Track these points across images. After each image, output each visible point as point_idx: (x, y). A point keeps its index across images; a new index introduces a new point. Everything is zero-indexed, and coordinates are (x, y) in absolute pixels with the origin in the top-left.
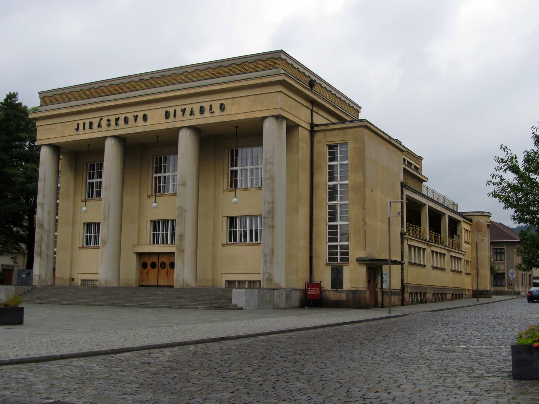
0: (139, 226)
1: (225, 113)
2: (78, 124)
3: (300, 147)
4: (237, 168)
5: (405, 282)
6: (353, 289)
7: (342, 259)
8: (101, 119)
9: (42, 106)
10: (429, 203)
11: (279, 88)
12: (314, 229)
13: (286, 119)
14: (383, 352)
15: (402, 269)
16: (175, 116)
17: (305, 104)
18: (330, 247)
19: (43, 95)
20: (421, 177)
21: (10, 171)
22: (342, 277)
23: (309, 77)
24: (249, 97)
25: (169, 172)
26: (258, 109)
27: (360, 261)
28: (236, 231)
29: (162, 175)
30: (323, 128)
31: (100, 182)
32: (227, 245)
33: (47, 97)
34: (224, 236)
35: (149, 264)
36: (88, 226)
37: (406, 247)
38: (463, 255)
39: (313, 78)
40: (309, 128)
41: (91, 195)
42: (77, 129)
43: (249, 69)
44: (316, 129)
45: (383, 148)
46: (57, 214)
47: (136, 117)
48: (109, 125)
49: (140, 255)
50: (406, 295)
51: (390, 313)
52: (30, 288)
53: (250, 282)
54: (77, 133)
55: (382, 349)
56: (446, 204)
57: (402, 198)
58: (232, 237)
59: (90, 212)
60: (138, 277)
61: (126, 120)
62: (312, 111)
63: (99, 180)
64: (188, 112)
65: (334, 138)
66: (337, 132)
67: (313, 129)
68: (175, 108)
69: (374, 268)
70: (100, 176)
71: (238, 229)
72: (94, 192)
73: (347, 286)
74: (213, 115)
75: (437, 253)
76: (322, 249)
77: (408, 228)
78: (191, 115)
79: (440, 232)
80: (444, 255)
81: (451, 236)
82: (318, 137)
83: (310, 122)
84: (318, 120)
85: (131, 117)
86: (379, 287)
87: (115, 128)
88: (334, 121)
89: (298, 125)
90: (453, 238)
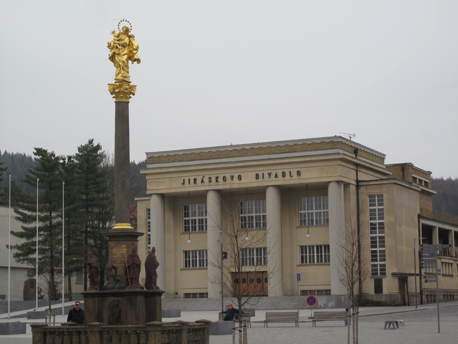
1: (301, 177)
2: (184, 180)
3: (351, 199)
7: (381, 274)
8: (203, 177)
11: (339, 162)
13: (342, 182)
16: (263, 178)
19: (150, 156)
22: (382, 286)
27: (394, 274)
30: (366, 183)
32: (300, 265)
35: (241, 280)
39: (356, 146)
40: (356, 184)
42: (184, 183)
44: (360, 184)
47: (232, 177)
48: (210, 181)
50: (424, 297)
51: (416, 308)
53: (318, 291)
54: (183, 186)
61: (224, 179)
62: (357, 171)
64: (273, 175)
65: (375, 191)
66: (375, 186)
67: (358, 184)
68: (262, 172)
69: (403, 279)
73: (385, 291)
75: (446, 263)
76: (368, 266)
78: (275, 177)
80: (452, 264)
82: (362, 190)
85: (228, 177)
86: (406, 292)
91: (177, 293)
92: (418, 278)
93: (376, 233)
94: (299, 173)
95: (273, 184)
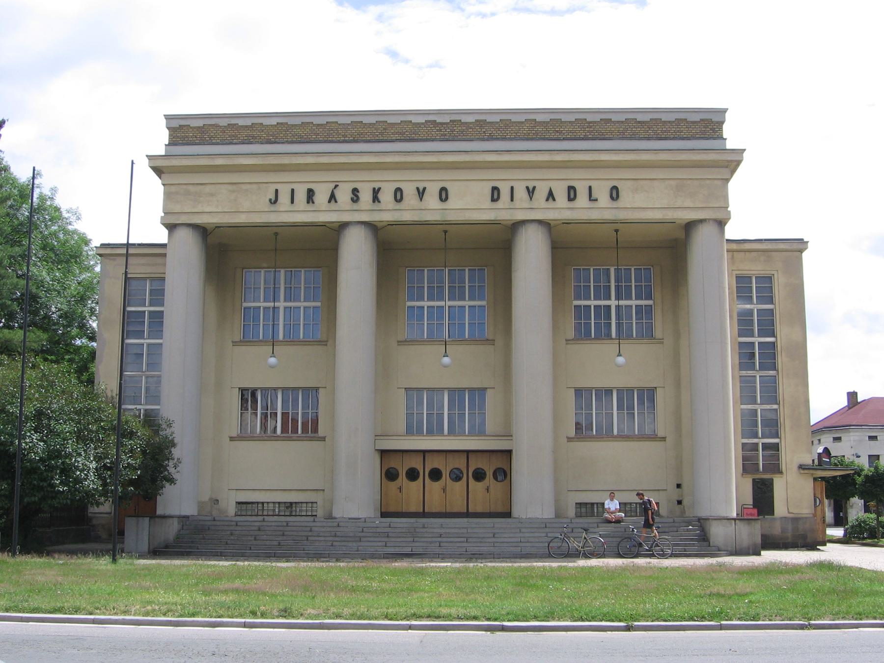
4: (277, 304)
8: (336, 186)
9: (172, 143)
19: (175, 124)
24: (667, 182)
25: (279, 301)
26: (686, 205)
35: (446, 474)
42: (274, 201)
47: (421, 193)
61: (398, 195)
73: (780, 509)
85: (409, 190)
87: (370, 207)
94: (615, 193)
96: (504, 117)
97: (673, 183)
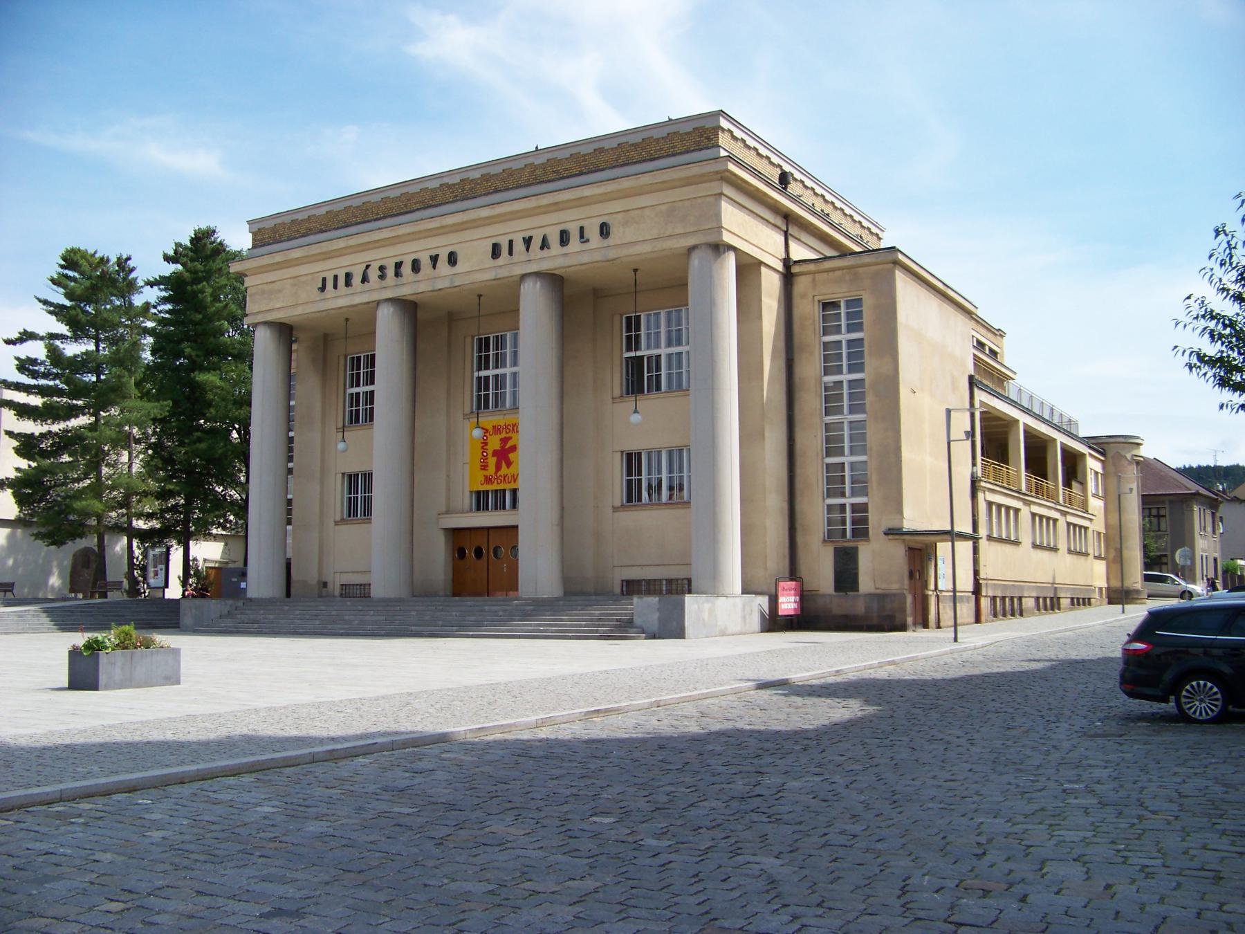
0: (448, 476)
1: (611, 241)
2: (324, 279)
5: (982, 575)
6: (879, 591)
8: (368, 267)
9: (254, 247)
10: (1024, 419)
12: (798, 471)
14: (963, 741)
15: (976, 550)
16: (511, 253)
17: (772, 220)
18: (830, 508)
20: (1004, 370)
21: (201, 377)
22: (857, 568)
23: (779, 166)
28: (640, 481)
29: (491, 373)
31: (372, 393)
33: (269, 234)
34: (617, 492)
36: (352, 478)
37: (982, 507)
38: (1091, 520)
40: (779, 266)
41: (354, 418)
42: (323, 289)
43: (656, 151)
45: (933, 305)
46: (290, 459)
48: (382, 277)
49: (455, 534)
50: (985, 603)
52: (240, 603)
55: (959, 733)
56: (1056, 420)
57: (972, 405)
58: (632, 494)
59: (351, 451)
60: (450, 576)
63: (369, 388)
67: (789, 272)
70: (371, 379)
71: (644, 477)
72: (360, 413)
73: (866, 584)
74: (586, 246)
77: (984, 467)
78: (542, 248)
79: (1045, 476)
81: (1067, 484)
83: (784, 256)
84: (799, 252)
86: (932, 587)
88: (829, 252)
89: (761, 263)
90: (1070, 487)
91: (325, 584)
92: (964, 548)
93: (841, 413)
95: (534, 268)
96: (505, 166)
97: (664, 208)
